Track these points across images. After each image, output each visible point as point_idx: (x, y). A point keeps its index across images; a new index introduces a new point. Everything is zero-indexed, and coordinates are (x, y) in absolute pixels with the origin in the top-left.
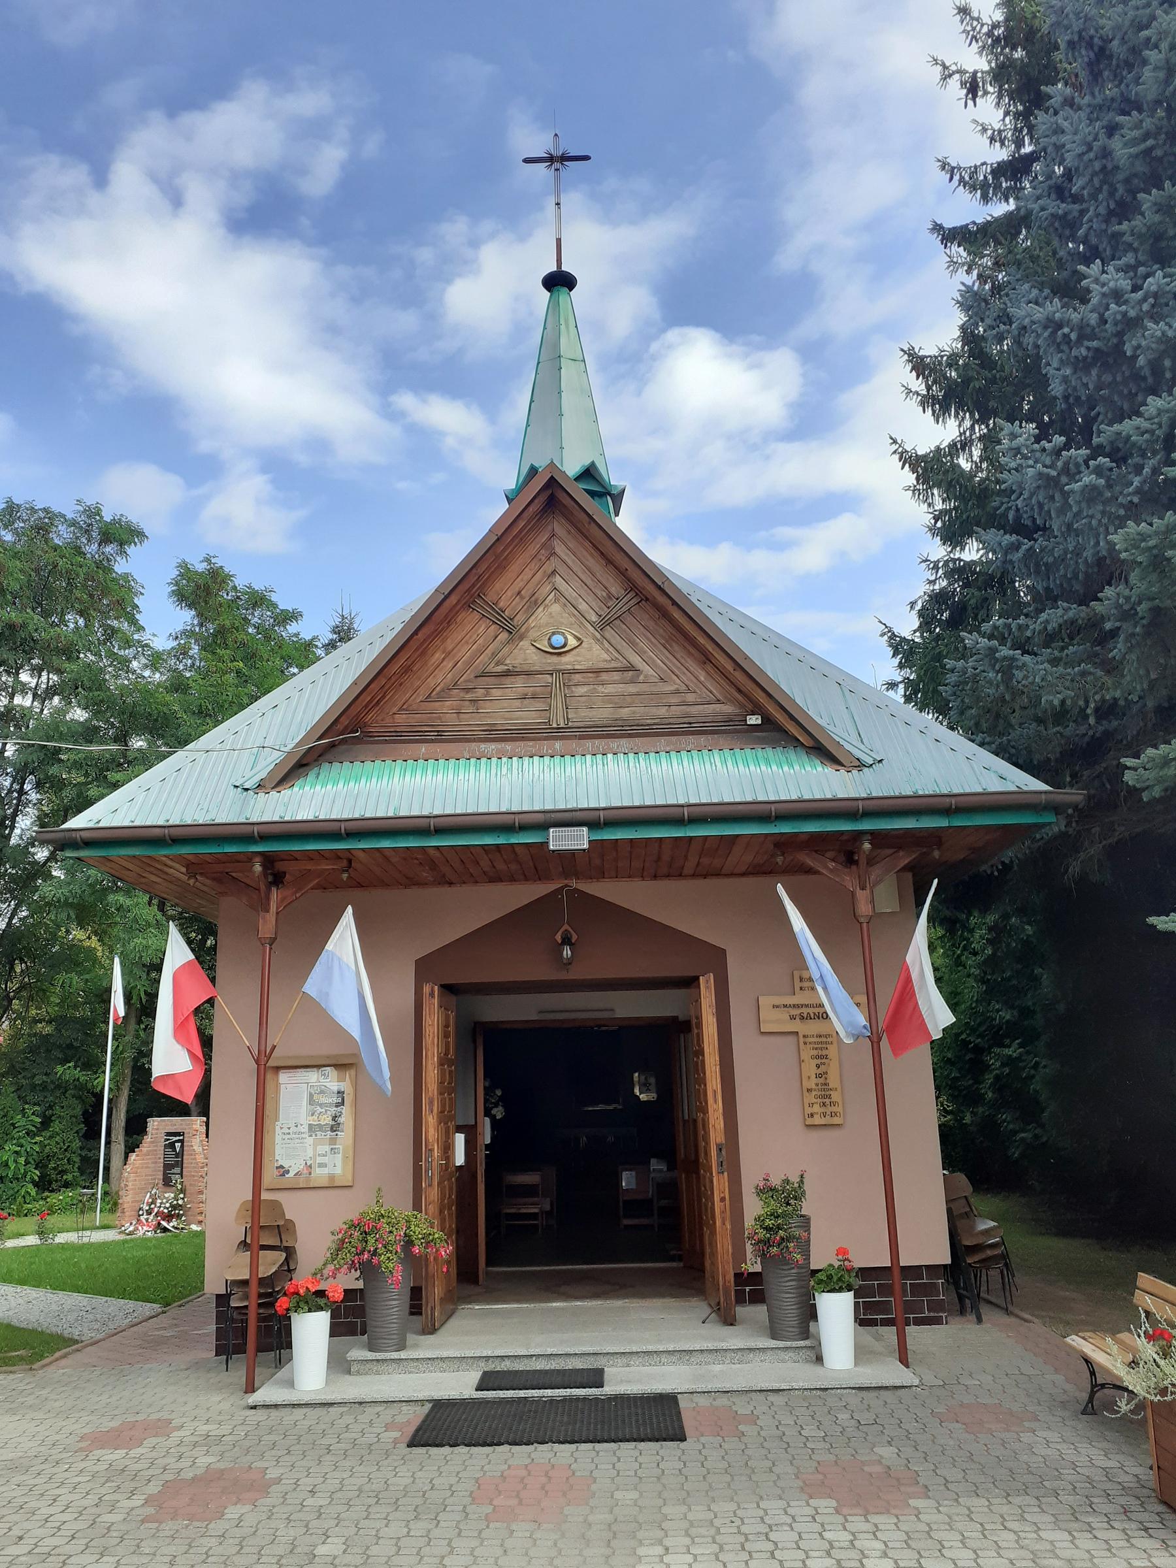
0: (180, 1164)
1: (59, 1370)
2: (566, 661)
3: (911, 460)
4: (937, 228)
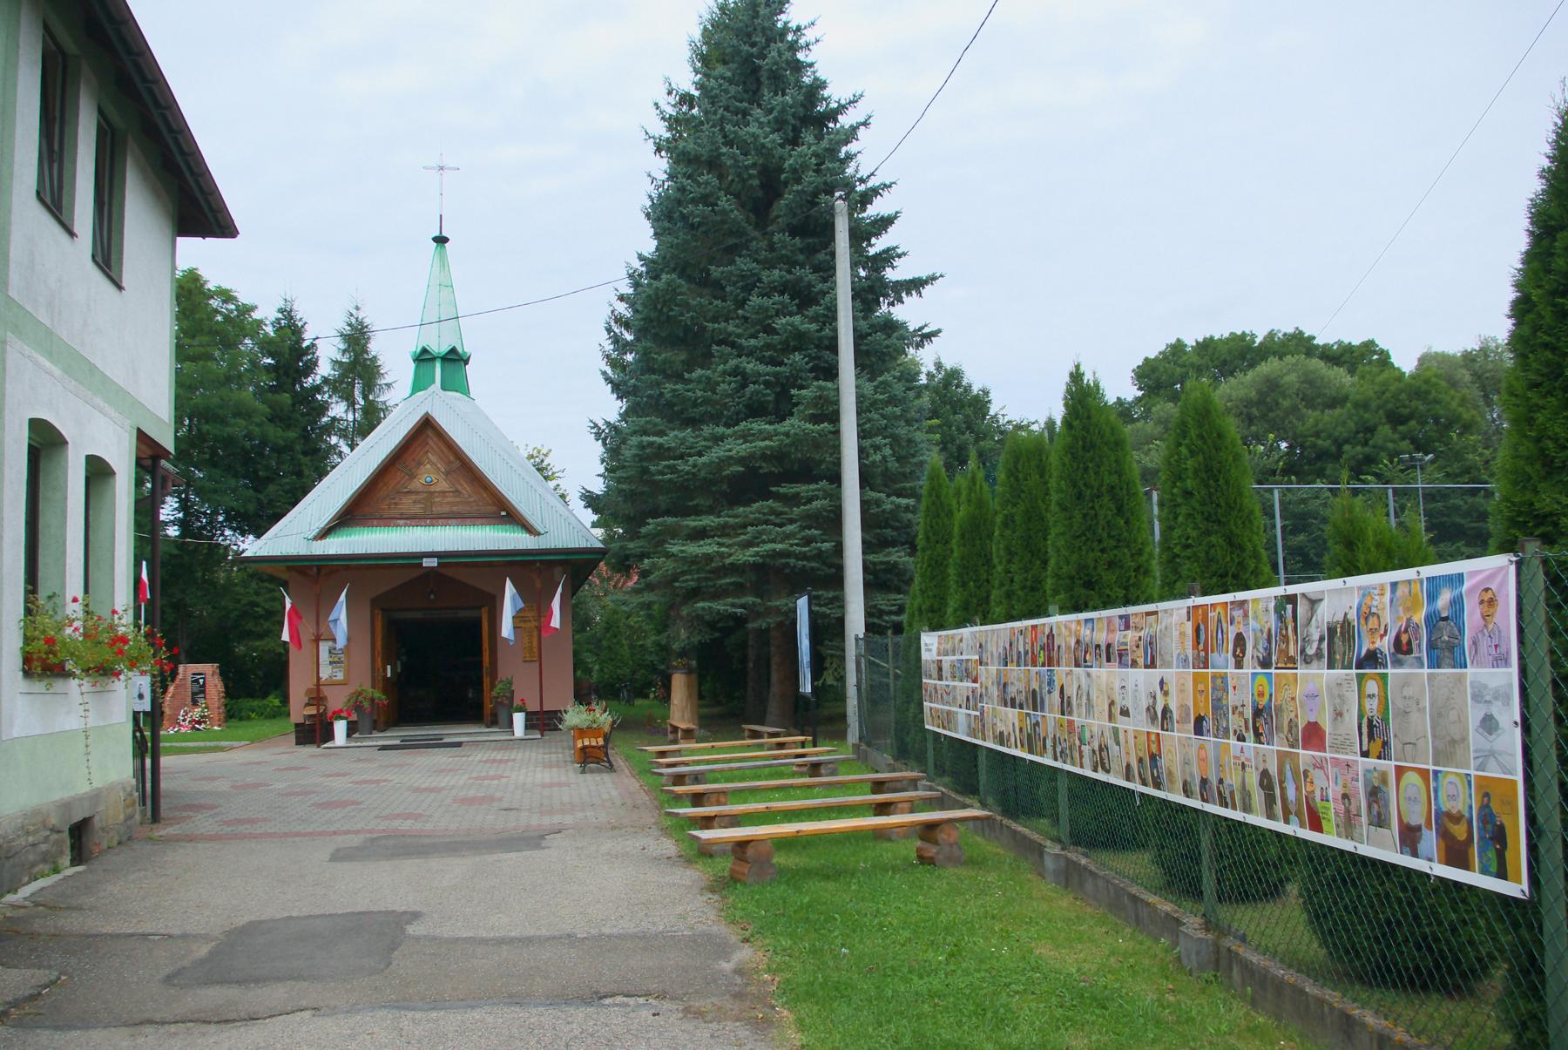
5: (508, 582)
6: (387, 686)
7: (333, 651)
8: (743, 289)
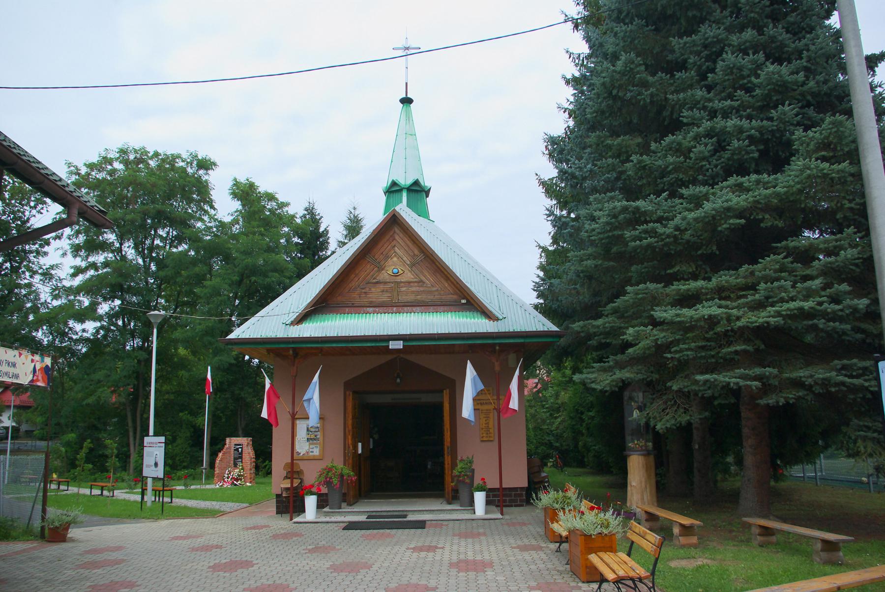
0: (241, 458)
1: (224, 518)
2: (398, 279)
3: (543, 183)
4: (564, 77)
5: (469, 367)
6: (357, 462)
7: (311, 427)
8: (708, 58)
